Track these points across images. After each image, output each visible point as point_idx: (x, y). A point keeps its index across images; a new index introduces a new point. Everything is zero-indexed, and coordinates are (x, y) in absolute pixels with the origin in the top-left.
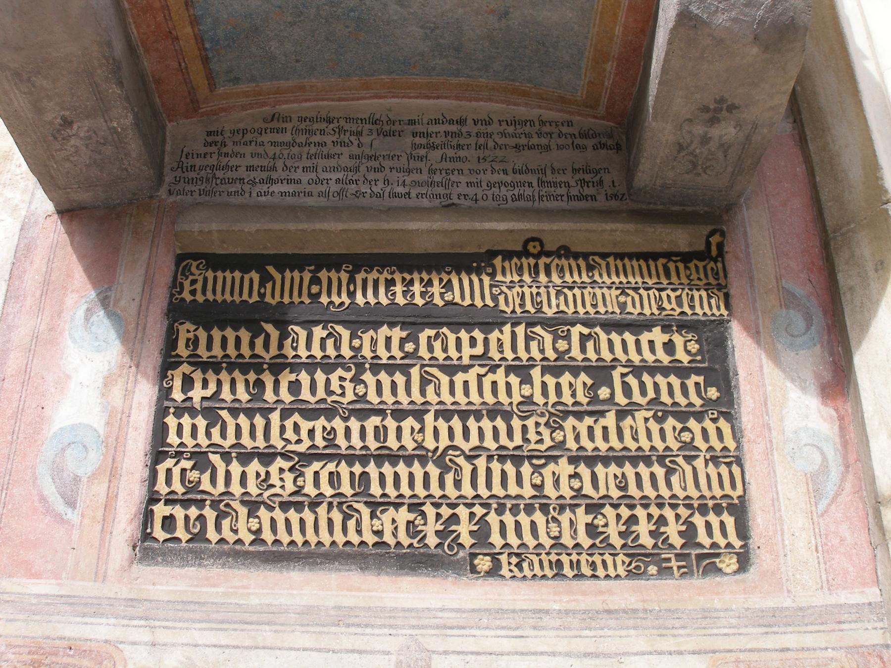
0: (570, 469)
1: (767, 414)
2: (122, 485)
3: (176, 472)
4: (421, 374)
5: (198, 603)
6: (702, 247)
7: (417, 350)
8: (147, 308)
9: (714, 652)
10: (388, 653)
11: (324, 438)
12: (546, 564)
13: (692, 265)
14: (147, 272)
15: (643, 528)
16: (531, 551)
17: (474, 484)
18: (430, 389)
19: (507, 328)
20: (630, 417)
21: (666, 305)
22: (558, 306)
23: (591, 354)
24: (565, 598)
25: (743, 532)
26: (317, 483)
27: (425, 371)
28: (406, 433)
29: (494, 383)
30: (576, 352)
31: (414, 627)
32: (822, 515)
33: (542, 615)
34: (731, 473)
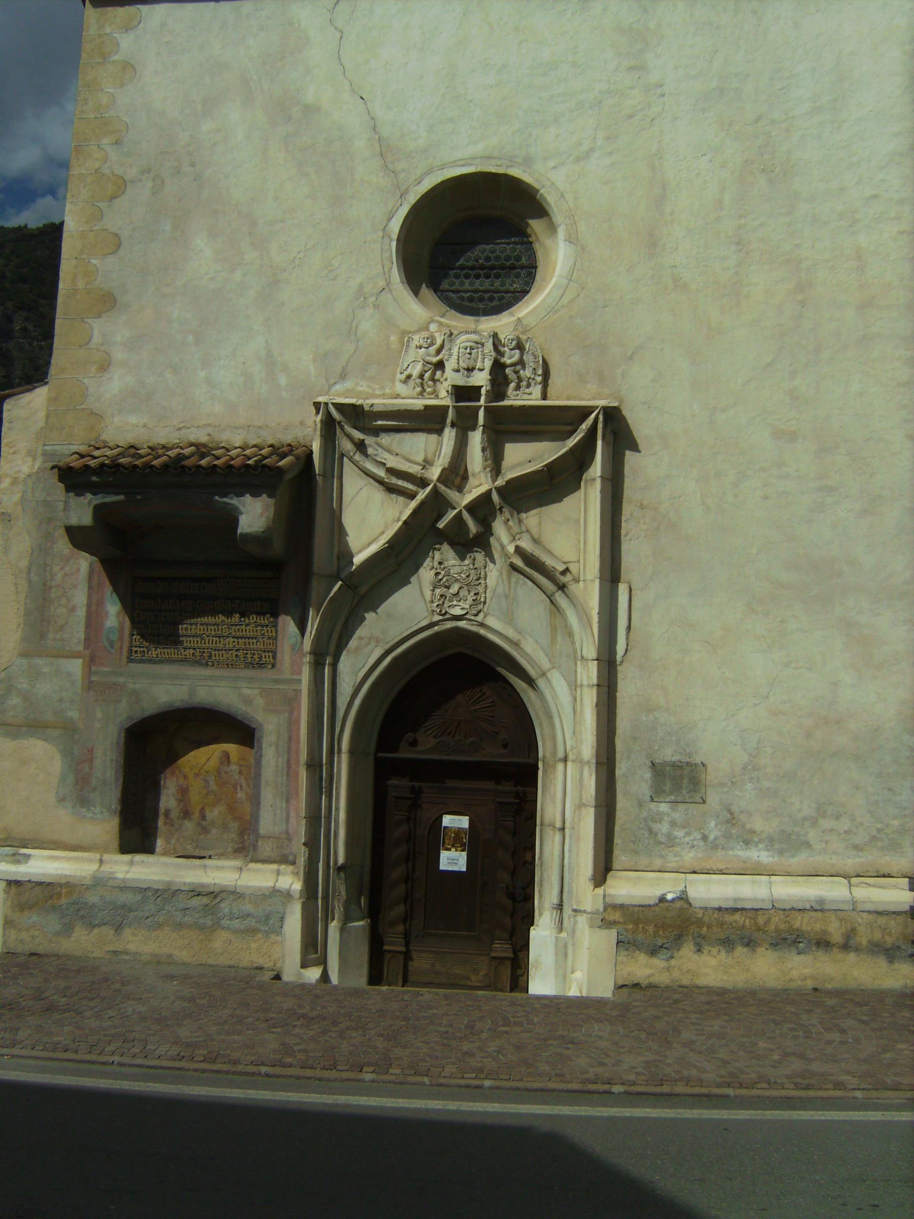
25: (274, 657)
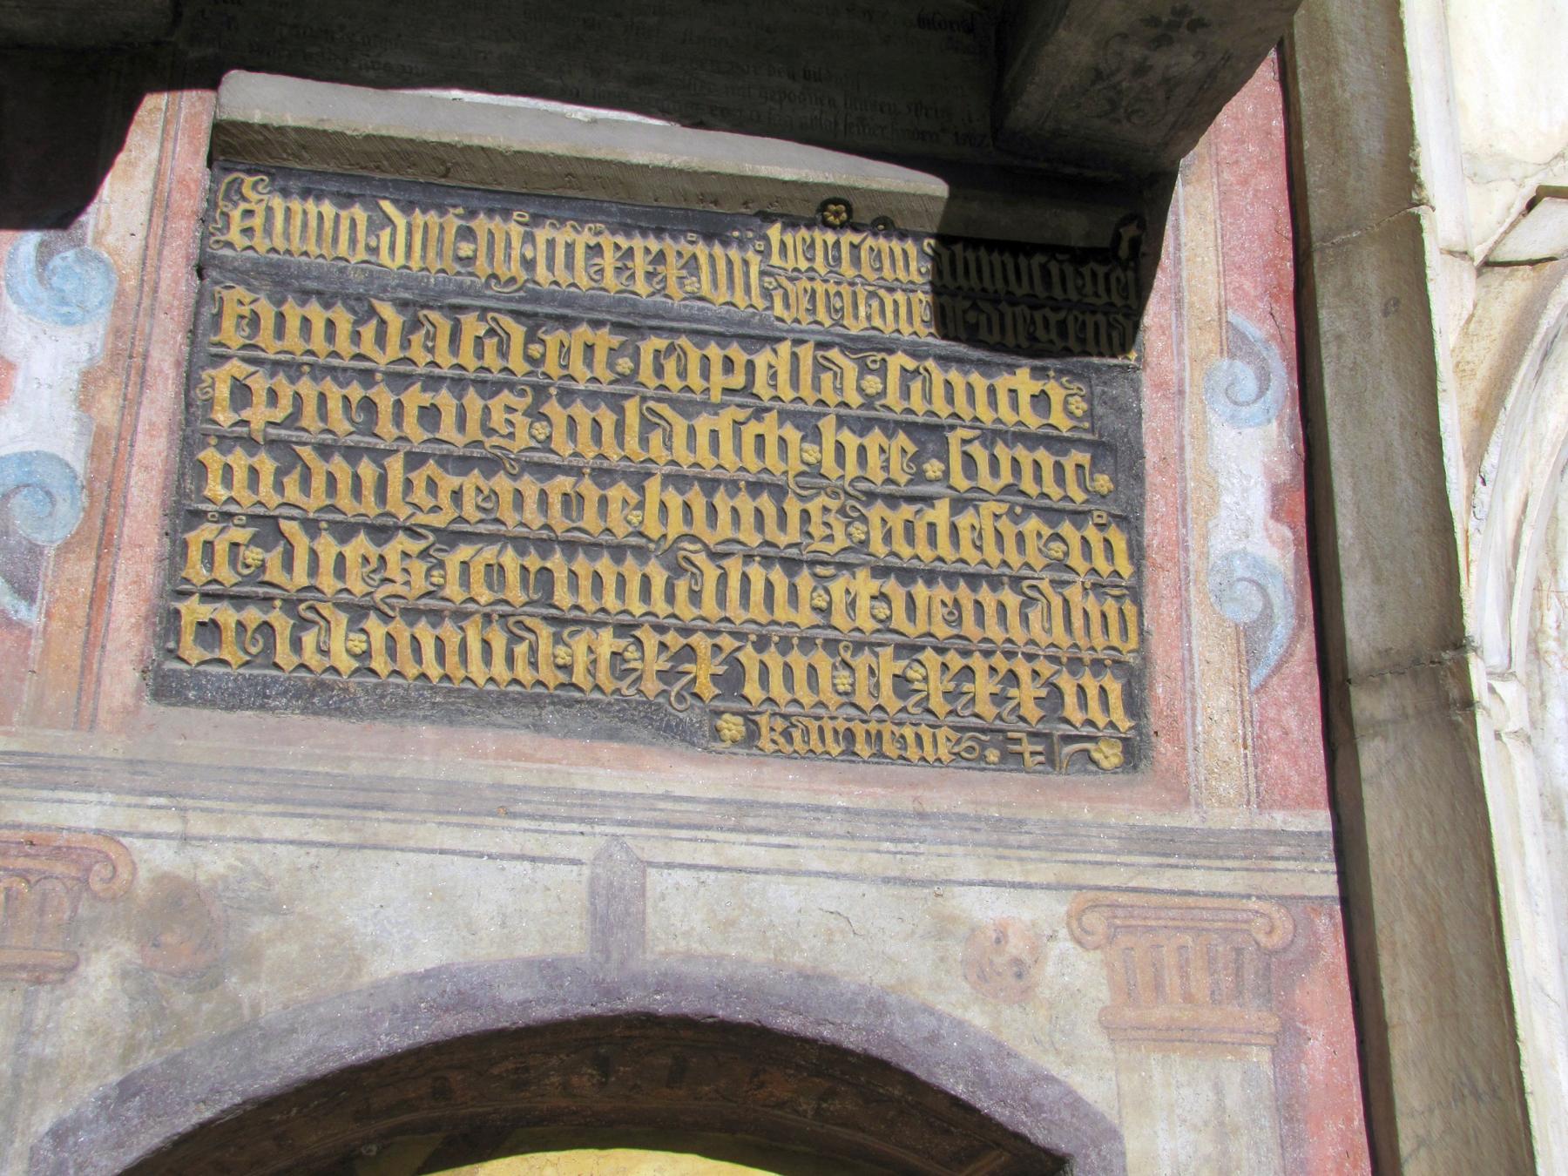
0: (874, 586)
1: (1185, 526)
2: (122, 566)
3: (221, 548)
4: (642, 416)
5: (262, 771)
6: (1106, 244)
7: (636, 371)
8: (160, 253)
9: (1080, 888)
10: (576, 862)
11: (478, 507)
12: (829, 735)
13: (1086, 271)
14: (155, 187)
15: (983, 686)
16: (807, 710)
17: (722, 601)
18: (656, 438)
19: (785, 348)
20: (971, 510)
21: (1041, 333)
22: (869, 317)
23: (917, 402)
24: (857, 790)
25: (1134, 706)
26: (465, 582)
27: (649, 409)
28: (614, 507)
29: (760, 438)
30: (893, 398)
31: (620, 823)
32: (1257, 691)
33: (820, 815)
34: (1121, 611)
